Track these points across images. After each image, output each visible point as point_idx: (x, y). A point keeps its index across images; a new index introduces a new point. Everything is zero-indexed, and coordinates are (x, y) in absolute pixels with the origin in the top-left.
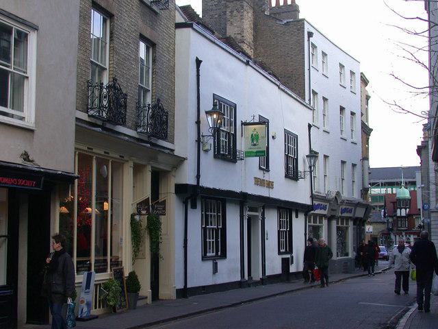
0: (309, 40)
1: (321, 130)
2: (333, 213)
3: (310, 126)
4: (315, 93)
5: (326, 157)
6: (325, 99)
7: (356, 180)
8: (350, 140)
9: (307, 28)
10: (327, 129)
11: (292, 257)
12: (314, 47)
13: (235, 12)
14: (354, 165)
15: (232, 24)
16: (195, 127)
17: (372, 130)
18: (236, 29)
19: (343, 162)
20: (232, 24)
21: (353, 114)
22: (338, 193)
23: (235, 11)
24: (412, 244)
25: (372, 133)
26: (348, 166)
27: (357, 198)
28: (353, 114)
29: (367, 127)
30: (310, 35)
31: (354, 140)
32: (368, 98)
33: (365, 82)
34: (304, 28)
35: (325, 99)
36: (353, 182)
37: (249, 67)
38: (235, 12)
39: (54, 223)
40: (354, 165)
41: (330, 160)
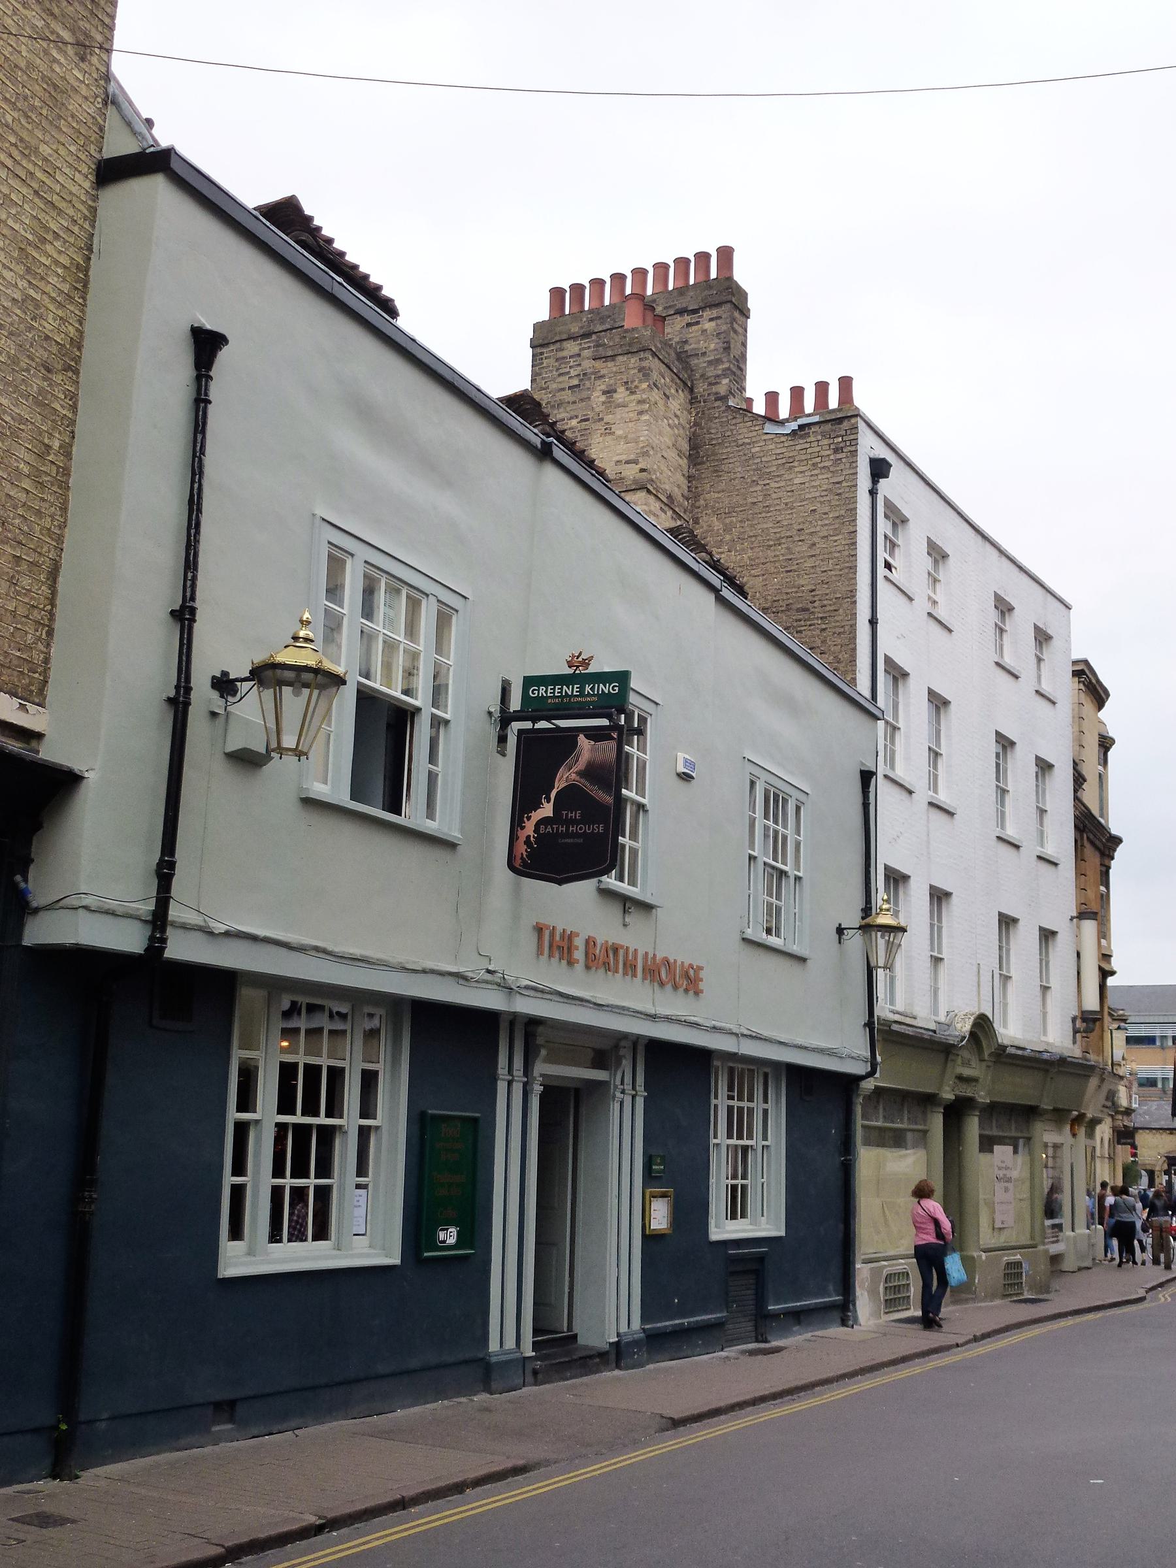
0: (873, 493)
1: (923, 795)
2: (967, 1091)
3: (867, 777)
4: (898, 675)
5: (939, 897)
6: (938, 703)
7: (1054, 983)
8: (1030, 849)
9: (868, 447)
10: (943, 797)
11: (278, 1172)
12: (898, 520)
13: (621, 394)
14: (1047, 936)
15: (608, 431)
16: (166, 636)
17: (1117, 841)
18: (622, 446)
19: (1007, 922)
20: (608, 431)
21: (1044, 767)
22: (982, 1024)
23: (621, 390)
24: (577, 672)
25: (1119, 852)
26: (1025, 939)
27: (1058, 1043)
28: (1044, 767)
29: (1102, 829)
30: (879, 469)
31: (1050, 851)
32: (1106, 744)
33: (1097, 693)
34: (854, 442)
35: (938, 703)
36: (1045, 989)
37: (551, 474)
38: (621, 394)
39: (659, 1328)
40: (1047, 936)
41: (955, 909)
